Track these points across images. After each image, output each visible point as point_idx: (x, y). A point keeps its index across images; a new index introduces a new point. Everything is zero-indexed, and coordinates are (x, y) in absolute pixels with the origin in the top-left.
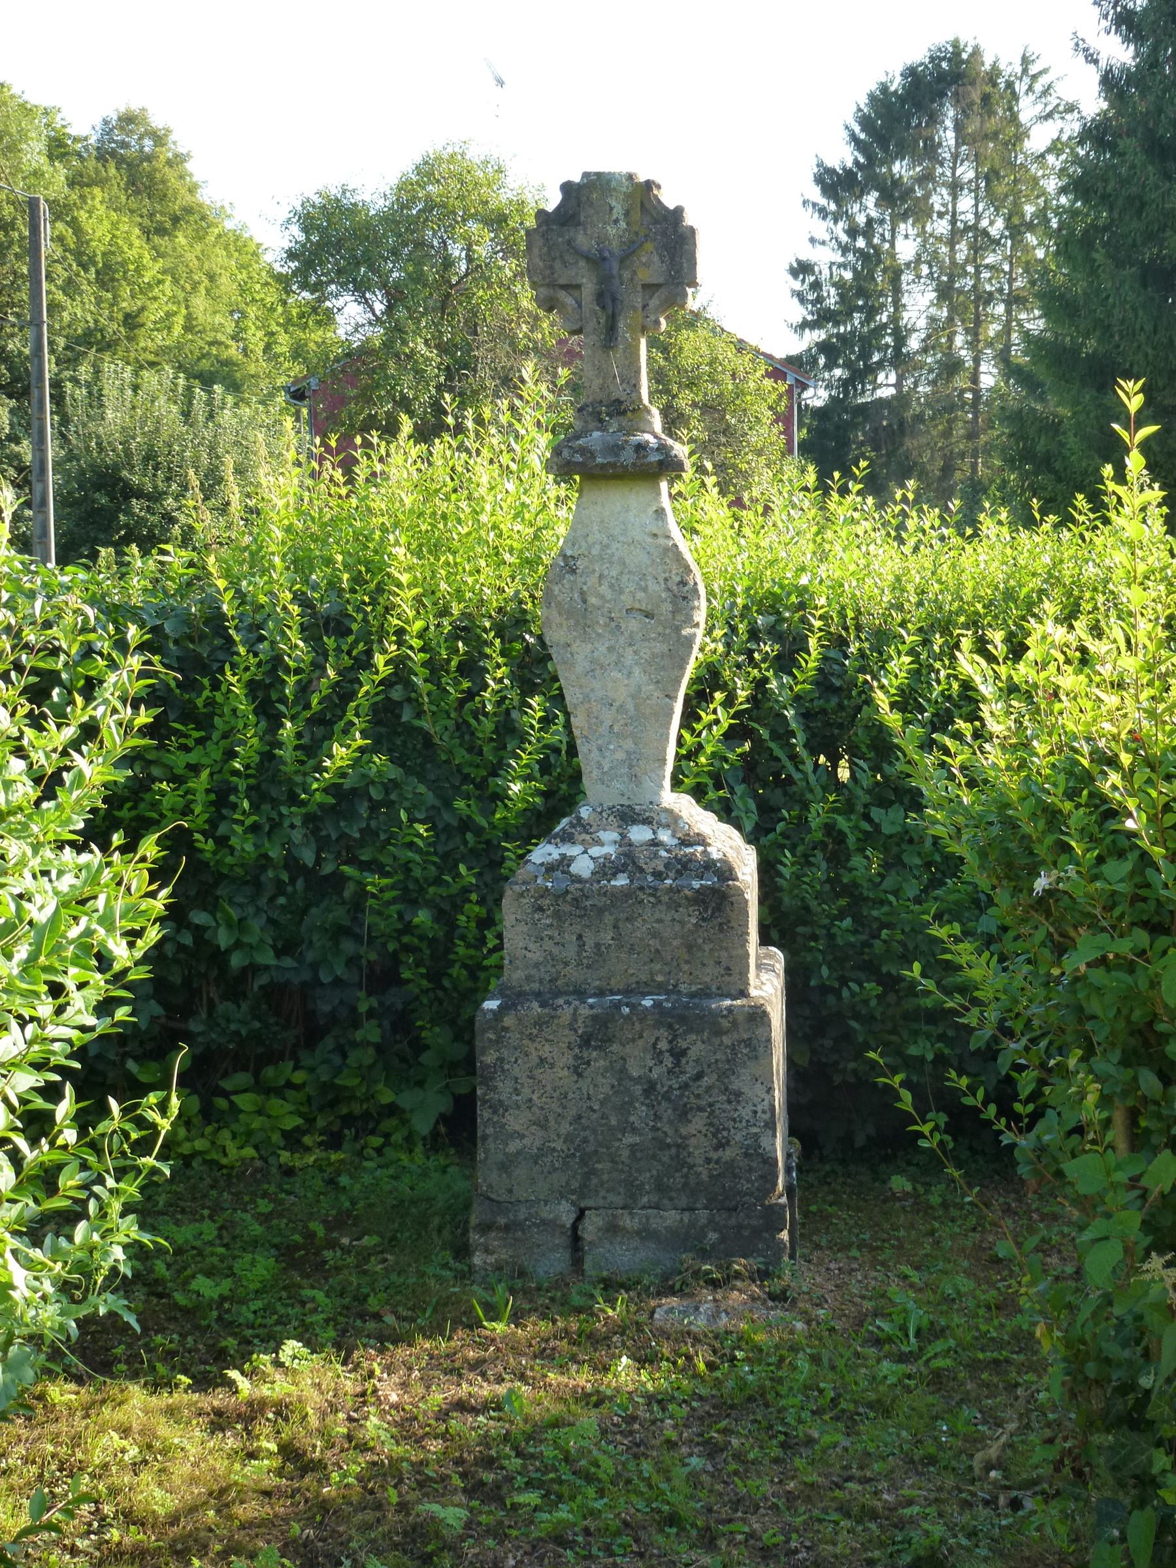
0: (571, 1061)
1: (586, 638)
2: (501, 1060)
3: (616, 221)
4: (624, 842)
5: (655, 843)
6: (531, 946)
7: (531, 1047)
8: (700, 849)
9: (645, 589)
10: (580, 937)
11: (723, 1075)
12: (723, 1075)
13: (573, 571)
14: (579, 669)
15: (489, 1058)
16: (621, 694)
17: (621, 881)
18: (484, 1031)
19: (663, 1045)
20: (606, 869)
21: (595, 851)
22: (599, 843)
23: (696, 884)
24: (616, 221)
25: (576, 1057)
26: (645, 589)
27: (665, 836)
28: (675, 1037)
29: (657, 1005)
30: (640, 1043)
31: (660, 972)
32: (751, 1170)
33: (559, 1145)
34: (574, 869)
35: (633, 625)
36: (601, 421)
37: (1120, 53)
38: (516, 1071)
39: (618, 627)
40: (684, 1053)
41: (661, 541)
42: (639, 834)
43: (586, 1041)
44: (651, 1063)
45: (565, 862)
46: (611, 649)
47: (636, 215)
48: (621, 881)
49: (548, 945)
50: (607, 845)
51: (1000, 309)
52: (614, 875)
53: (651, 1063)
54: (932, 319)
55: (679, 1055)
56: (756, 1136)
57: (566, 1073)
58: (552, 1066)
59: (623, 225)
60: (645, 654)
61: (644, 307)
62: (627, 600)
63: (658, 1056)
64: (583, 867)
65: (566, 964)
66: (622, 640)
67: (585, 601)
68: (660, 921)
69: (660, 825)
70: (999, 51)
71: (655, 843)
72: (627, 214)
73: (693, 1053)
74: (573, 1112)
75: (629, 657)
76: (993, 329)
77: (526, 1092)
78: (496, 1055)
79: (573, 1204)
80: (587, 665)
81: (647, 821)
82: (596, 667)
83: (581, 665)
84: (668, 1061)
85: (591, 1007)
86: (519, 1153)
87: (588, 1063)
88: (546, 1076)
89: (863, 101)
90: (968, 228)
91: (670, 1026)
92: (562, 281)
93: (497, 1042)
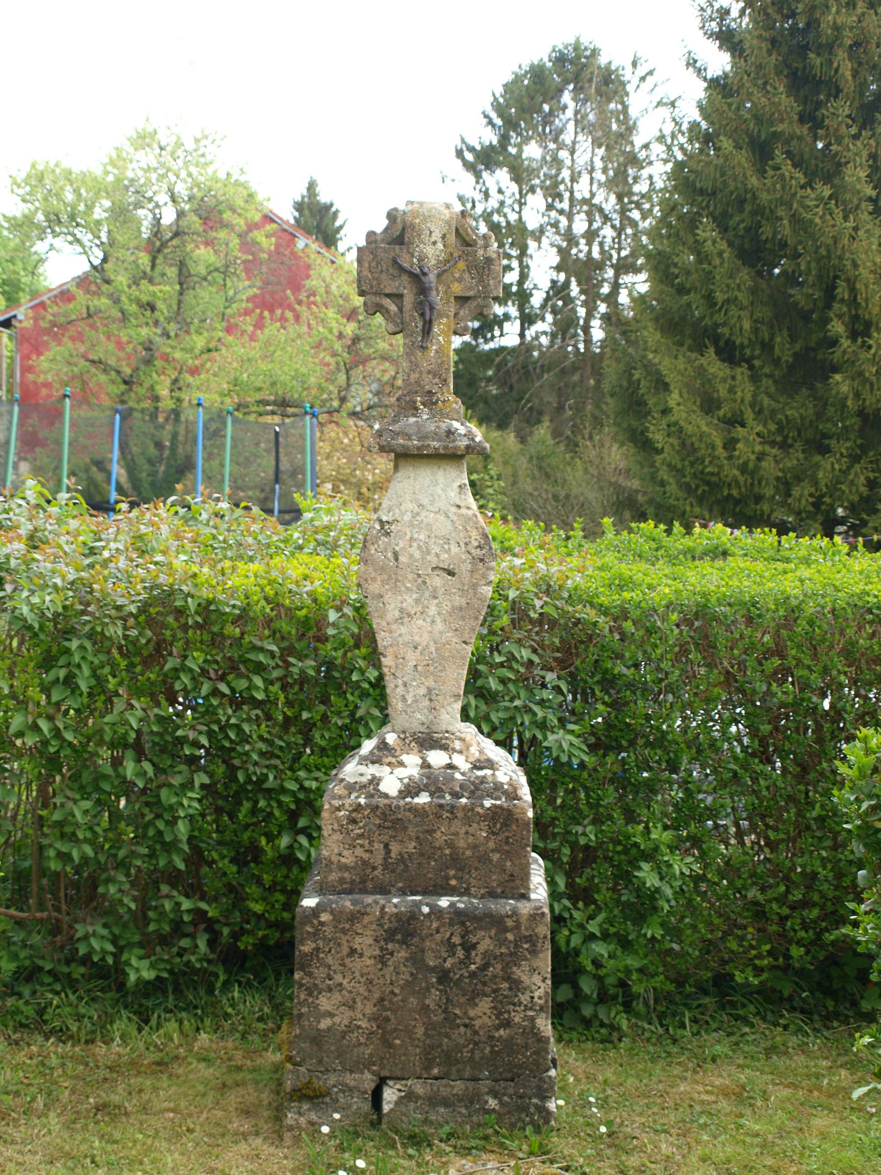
0: (377, 952)
1: (395, 590)
2: (317, 949)
3: (434, 243)
4: (426, 765)
5: (451, 766)
6: (345, 853)
7: (344, 939)
8: (488, 772)
9: (448, 551)
10: (386, 846)
11: (506, 966)
12: (506, 966)
13: (387, 534)
14: (389, 617)
15: (307, 947)
16: (423, 639)
17: (423, 799)
18: (303, 924)
19: (456, 940)
20: (410, 790)
21: (401, 772)
22: (401, 764)
23: (488, 803)
24: (434, 243)
25: (382, 949)
26: (448, 551)
27: (459, 760)
28: (467, 932)
29: (452, 904)
30: (438, 937)
31: (455, 877)
32: (527, 1047)
33: (364, 1024)
34: (383, 787)
35: (438, 581)
36: (417, 409)
37: (719, 62)
38: (330, 960)
39: (424, 583)
40: (474, 946)
41: (464, 511)
42: (438, 758)
43: (390, 935)
44: (445, 955)
45: (375, 781)
46: (417, 601)
47: (452, 238)
48: (423, 799)
49: (359, 852)
50: (411, 764)
51: (610, 273)
52: (417, 794)
53: (445, 955)
54: (554, 282)
55: (469, 948)
56: (532, 1019)
57: (372, 961)
58: (361, 955)
59: (440, 246)
60: (446, 606)
61: (456, 315)
62: (435, 561)
63: (451, 948)
64: (391, 785)
65: (374, 868)
66: (427, 594)
67: (397, 559)
68: (456, 834)
69: (454, 750)
70: (614, 55)
71: (451, 766)
72: (444, 237)
73: (482, 947)
74: (377, 995)
75: (433, 610)
76: (605, 289)
77: (338, 978)
78: (313, 945)
79: (373, 1073)
80: (397, 614)
81: (445, 748)
82: (405, 615)
83: (393, 613)
84: (460, 953)
85: (396, 906)
86: (329, 1029)
87: (392, 954)
88: (356, 964)
89: (499, 91)
90: (585, 201)
91: (463, 924)
92: (387, 291)
93: (315, 934)
